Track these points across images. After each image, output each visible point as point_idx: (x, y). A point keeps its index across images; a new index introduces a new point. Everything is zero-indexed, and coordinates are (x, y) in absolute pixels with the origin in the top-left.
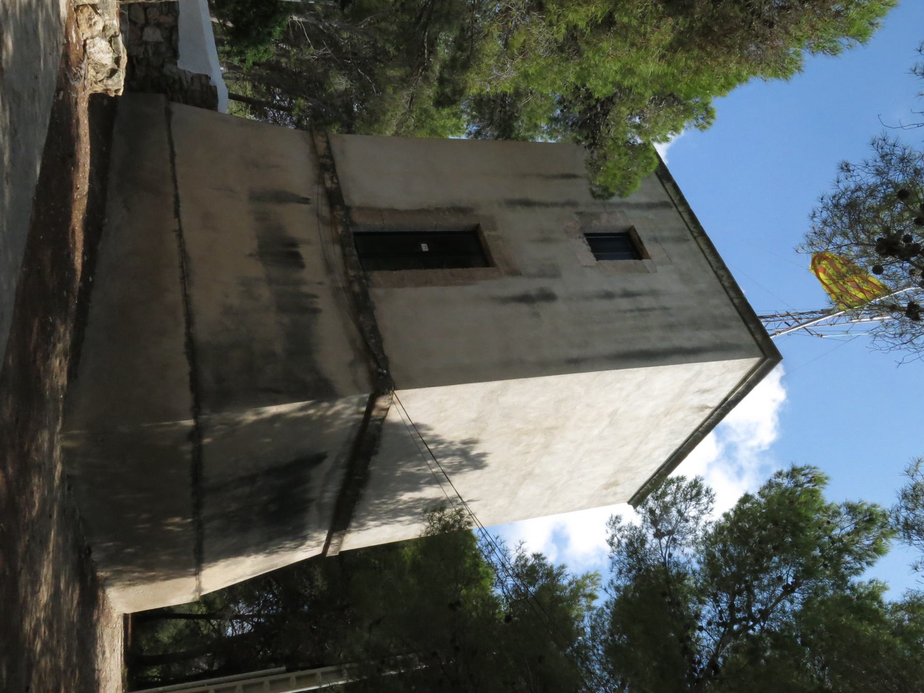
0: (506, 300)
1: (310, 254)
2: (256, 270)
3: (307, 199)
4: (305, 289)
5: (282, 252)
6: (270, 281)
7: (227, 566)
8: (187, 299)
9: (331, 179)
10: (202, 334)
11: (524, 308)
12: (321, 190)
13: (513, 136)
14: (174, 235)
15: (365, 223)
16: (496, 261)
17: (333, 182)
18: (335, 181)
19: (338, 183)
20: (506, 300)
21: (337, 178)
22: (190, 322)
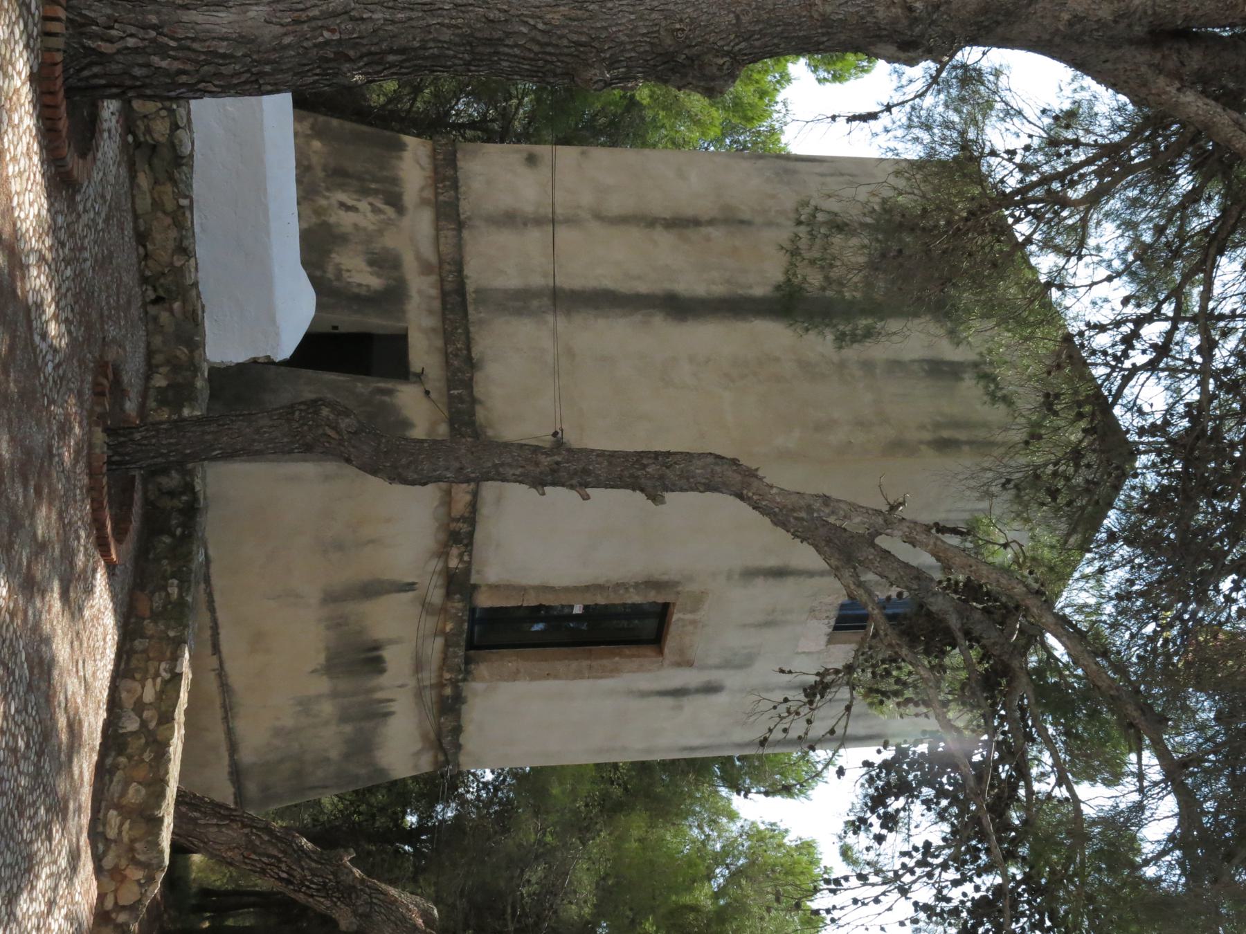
0: (644, 694)
1: (397, 660)
2: (323, 685)
3: (414, 584)
4: (379, 695)
5: (362, 658)
6: (334, 695)
7: (327, 478)
8: (230, 732)
9: (461, 555)
10: (247, 756)
11: (669, 701)
12: (440, 565)
13: (443, 223)
14: (212, 675)
15: (484, 601)
16: (666, 651)
17: (461, 560)
18: (466, 558)
19: (470, 563)
20: (644, 694)
21: (470, 555)
22: (233, 748)
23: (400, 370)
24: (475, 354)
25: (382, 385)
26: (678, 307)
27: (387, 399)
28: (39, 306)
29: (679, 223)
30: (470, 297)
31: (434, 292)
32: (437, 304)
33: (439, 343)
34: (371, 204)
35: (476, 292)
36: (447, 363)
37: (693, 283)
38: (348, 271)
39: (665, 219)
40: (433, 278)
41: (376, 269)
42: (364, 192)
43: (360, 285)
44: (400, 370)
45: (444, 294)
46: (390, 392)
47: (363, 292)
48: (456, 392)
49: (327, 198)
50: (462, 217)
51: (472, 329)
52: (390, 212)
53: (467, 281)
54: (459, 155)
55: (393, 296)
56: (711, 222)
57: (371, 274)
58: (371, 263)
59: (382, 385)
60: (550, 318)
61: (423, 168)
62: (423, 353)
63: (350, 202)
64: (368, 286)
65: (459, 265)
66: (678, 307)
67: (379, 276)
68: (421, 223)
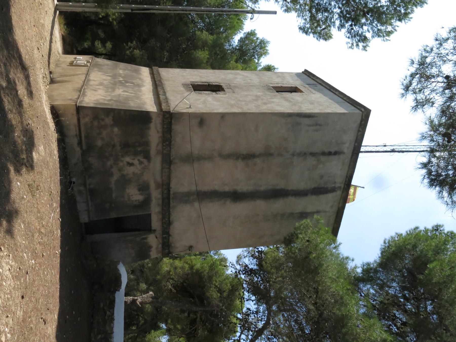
23: (150, 230)
24: (171, 219)
25: (144, 237)
26: (236, 196)
27: (145, 241)
28: (150, 247)
29: (248, 157)
30: (171, 196)
31: (160, 196)
32: (160, 201)
33: (161, 216)
34: (139, 160)
35: (174, 194)
36: (163, 226)
37: (244, 187)
38: (132, 195)
39: (243, 155)
40: (160, 190)
41: (141, 192)
42: (136, 154)
43: (136, 200)
44: (150, 230)
45: (163, 199)
46: (146, 238)
47: (137, 203)
48: (164, 236)
49: (122, 161)
50: (172, 158)
51: (171, 210)
52: (145, 161)
53: (171, 190)
54: (173, 121)
55: (146, 202)
56: (259, 156)
57: (140, 194)
58: (139, 190)
59: (144, 237)
60: (196, 205)
61: (158, 132)
62: (156, 223)
63: (131, 161)
64: (139, 200)
65: (168, 185)
66: (236, 196)
67: (141, 194)
68: (156, 163)
